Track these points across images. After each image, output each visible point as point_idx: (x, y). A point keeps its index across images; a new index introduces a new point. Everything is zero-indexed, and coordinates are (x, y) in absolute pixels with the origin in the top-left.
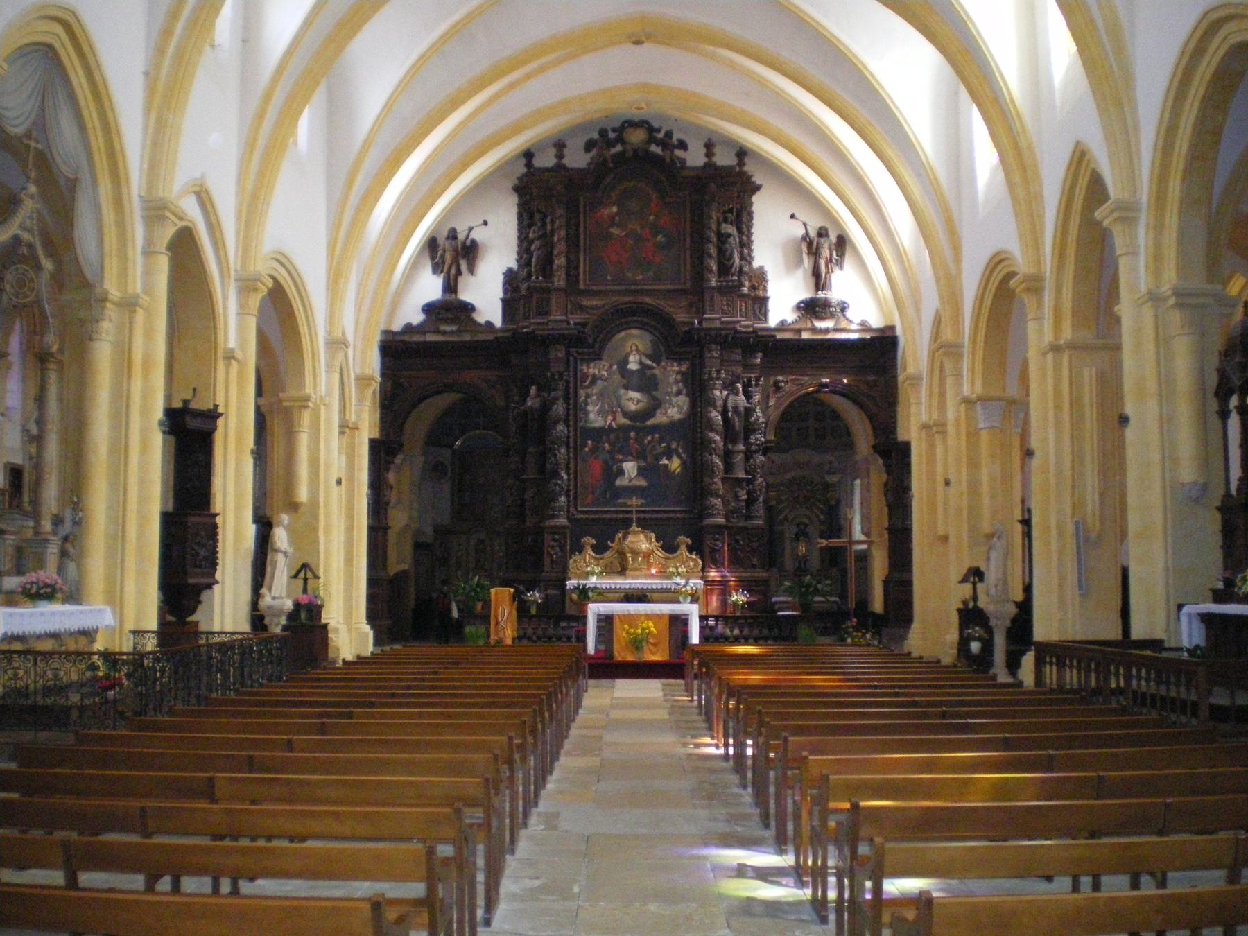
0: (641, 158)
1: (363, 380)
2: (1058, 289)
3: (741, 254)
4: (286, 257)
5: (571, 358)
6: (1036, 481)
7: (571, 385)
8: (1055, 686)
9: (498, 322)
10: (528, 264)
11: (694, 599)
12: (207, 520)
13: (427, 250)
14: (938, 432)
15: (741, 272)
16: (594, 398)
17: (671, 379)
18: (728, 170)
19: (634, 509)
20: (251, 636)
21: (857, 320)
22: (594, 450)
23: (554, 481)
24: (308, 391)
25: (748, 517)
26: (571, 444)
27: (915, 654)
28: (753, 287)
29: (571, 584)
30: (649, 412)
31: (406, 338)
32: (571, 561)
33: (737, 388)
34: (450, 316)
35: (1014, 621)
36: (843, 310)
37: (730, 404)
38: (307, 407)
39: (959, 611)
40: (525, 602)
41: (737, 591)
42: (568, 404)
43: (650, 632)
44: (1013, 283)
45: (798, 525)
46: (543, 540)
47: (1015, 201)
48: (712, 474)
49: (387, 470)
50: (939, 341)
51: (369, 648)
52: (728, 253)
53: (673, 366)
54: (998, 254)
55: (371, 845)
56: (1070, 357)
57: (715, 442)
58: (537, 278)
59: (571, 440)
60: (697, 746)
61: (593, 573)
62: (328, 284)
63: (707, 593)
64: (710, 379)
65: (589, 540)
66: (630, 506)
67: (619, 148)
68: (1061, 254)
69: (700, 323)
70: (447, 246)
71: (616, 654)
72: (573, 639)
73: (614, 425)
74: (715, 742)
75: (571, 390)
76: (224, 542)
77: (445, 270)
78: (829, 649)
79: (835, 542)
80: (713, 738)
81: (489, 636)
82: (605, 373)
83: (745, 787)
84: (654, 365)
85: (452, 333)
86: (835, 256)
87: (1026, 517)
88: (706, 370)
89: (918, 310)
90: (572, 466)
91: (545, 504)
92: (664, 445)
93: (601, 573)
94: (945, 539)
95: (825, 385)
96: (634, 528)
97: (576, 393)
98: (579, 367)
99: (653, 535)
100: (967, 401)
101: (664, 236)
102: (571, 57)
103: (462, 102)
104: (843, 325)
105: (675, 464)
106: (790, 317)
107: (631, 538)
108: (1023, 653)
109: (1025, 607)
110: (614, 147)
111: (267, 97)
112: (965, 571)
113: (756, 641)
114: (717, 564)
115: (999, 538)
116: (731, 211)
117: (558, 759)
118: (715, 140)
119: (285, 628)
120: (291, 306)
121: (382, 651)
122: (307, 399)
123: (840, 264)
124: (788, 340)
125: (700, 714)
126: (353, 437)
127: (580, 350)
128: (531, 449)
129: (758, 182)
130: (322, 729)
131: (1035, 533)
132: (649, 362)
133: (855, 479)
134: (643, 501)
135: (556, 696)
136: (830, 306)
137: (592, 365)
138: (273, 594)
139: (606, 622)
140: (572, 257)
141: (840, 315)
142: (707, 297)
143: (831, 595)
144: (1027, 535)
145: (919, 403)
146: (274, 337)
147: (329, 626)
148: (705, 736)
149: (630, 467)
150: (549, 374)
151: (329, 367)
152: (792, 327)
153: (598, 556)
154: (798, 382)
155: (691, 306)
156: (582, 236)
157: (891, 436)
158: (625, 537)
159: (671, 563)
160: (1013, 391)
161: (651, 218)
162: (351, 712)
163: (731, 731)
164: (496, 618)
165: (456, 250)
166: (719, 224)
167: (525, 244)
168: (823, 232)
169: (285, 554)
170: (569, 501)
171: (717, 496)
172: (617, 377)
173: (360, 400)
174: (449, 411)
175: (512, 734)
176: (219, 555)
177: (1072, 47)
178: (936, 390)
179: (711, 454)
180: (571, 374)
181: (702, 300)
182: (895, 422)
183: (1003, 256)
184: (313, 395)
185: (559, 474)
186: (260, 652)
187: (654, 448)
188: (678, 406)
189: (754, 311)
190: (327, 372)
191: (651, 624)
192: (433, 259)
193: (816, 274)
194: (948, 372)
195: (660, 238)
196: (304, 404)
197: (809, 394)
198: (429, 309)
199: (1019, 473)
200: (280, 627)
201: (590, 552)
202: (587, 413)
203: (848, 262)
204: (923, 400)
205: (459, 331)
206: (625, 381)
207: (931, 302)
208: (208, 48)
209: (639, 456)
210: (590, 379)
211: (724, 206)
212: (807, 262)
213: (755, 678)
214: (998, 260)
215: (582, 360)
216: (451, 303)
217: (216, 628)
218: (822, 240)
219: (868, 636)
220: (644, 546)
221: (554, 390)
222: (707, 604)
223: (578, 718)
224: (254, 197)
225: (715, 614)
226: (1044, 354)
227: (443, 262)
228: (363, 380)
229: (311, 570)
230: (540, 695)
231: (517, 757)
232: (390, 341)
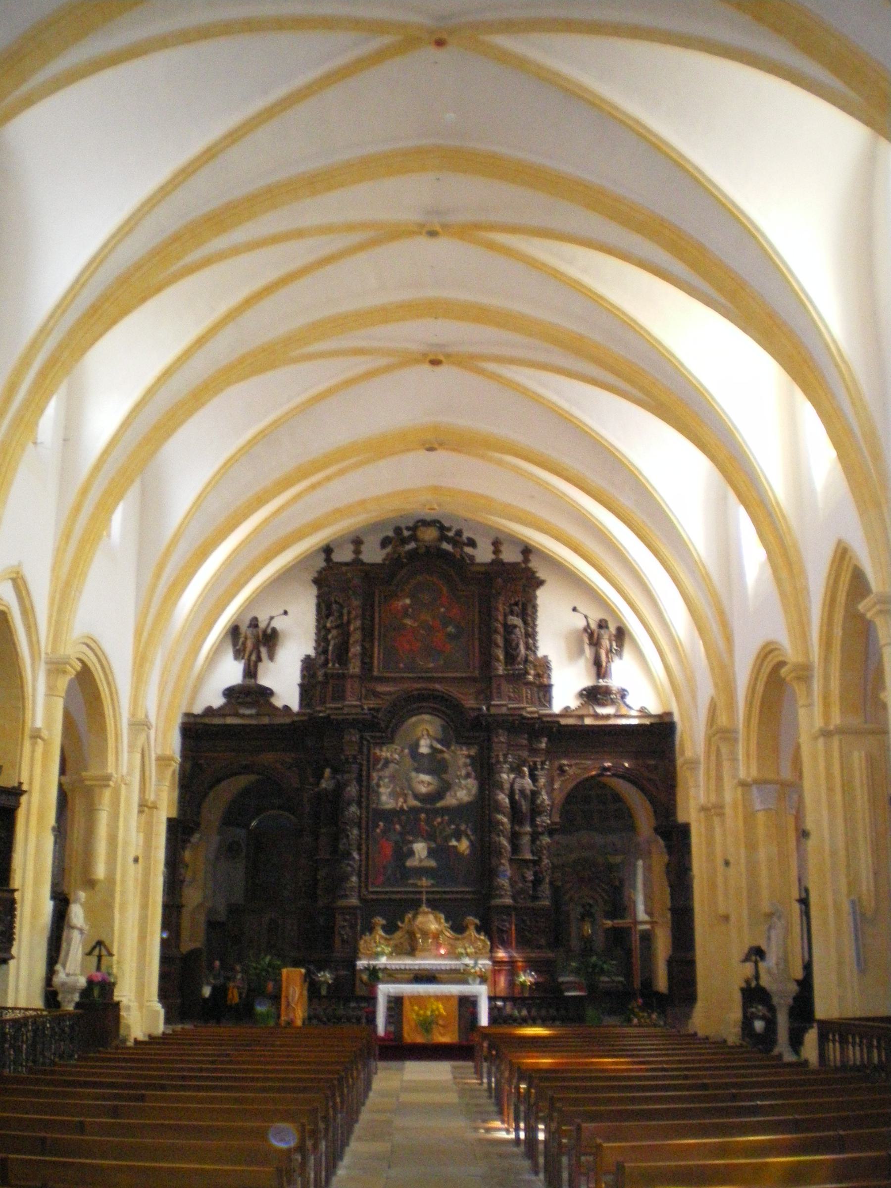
1: (163, 760)
2: (826, 678)
4: (95, 642)
5: (365, 743)
6: (812, 862)
7: (365, 768)
8: (838, 1064)
9: (295, 706)
10: (325, 652)
11: (483, 979)
12: (5, 895)
13: (230, 636)
15: (526, 661)
16: (386, 780)
18: (515, 565)
20: (45, 1013)
22: (384, 832)
23: (346, 862)
25: (535, 898)
27: (701, 1034)
28: (538, 675)
29: (361, 963)
30: (439, 795)
31: (207, 720)
32: (362, 942)
33: (523, 772)
35: (795, 999)
36: (623, 697)
37: (517, 787)
38: (108, 786)
39: (743, 990)
41: (525, 972)
42: (361, 786)
44: (783, 671)
45: (583, 906)
47: (783, 594)
49: (183, 848)
50: (715, 727)
51: (160, 1028)
52: (514, 644)
53: (461, 750)
54: (764, 648)
55: (448, 889)
56: (841, 741)
57: (502, 824)
58: (334, 665)
60: (488, 1130)
61: (382, 953)
63: (496, 973)
64: (498, 762)
65: (380, 921)
66: (422, 887)
68: (827, 643)
69: (488, 709)
70: (249, 635)
71: (405, 1035)
72: (364, 1020)
73: (405, 807)
74: (506, 1126)
75: (364, 773)
76: (21, 916)
78: (617, 1030)
79: (619, 922)
80: (503, 1122)
81: (279, 1016)
82: (396, 756)
83: (536, 1173)
84: (444, 749)
86: (614, 646)
87: (804, 895)
88: (493, 755)
89: (694, 697)
90: (364, 847)
91: (337, 884)
92: (453, 827)
93: (391, 953)
94: (726, 918)
96: (424, 908)
97: (369, 777)
98: (372, 751)
99: (442, 916)
100: (743, 784)
102: (368, 461)
103: (267, 501)
104: (624, 711)
105: (464, 846)
106: (574, 703)
107: (420, 919)
108: (804, 1030)
109: (806, 984)
110: (408, 544)
111: (85, 491)
112: (746, 950)
113: (544, 1022)
114: (505, 944)
115: (779, 918)
117: (348, 1144)
119: (78, 1005)
121: (174, 1031)
122: (108, 778)
123: (619, 653)
124: (571, 726)
125: (490, 1097)
126: (151, 816)
130: (115, 1112)
131: (814, 912)
132: (439, 746)
134: (432, 882)
135: (348, 1081)
137: (384, 749)
138: (67, 971)
139: (396, 1003)
142: (494, 685)
143: (616, 975)
144: (806, 913)
145: (697, 786)
146: (81, 719)
147: (121, 1005)
148: (496, 1120)
149: (420, 848)
150: (343, 757)
151: (131, 747)
153: (388, 937)
154: (582, 766)
157: (672, 818)
158: (415, 917)
159: (459, 943)
160: (787, 774)
162: (143, 1095)
163: (522, 1115)
164: (287, 997)
165: (257, 637)
166: (505, 616)
167: (323, 633)
168: (603, 624)
169: (81, 931)
170: (360, 881)
172: (408, 761)
173: (160, 780)
174: (246, 792)
175: (304, 1120)
176: (16, 931)
177: (832, 453)
178: (713, 774)
179: (499, 835)
180: (365, 758)
181: (489, 687)
183: (772, 647)
186: (52, 1028)
188: (467, 788)
189: (539, 698)
190: (129, 752)
191: (441, 1006)
192: (235, 644)
193: (597, 663)
194: (724, 757)
195: (451, 629)
196: (105, 783)
197: (593, 777)
198: (230, 693)
199: (795, 853)
200: (73, 1004)
201: (381, 932)
202: (378, 795)
203: (628, 653)
204: (702, 784)
205: (258, 715)
206: (416, 765)
207: (706, 690)
208: (31, 445)
209: (429, 837)
212: (588, 652)
213: (546, 1061)
214: (768, 651)
215: (376, 744)
217: (10, 1004)
218: (602, 631)
219: (654, 1016)
220: (434, 926)
221: (349, 772)
222: (495, 984)
223: (369, 1102)
224: (68, 584)
225: (502, 994)
226: (815, 738)
227: (244, 650)
228: (163, 760)
229: (105, 947)
230: (332, 1079)
231: (309, 1144)
232: (189, 724)
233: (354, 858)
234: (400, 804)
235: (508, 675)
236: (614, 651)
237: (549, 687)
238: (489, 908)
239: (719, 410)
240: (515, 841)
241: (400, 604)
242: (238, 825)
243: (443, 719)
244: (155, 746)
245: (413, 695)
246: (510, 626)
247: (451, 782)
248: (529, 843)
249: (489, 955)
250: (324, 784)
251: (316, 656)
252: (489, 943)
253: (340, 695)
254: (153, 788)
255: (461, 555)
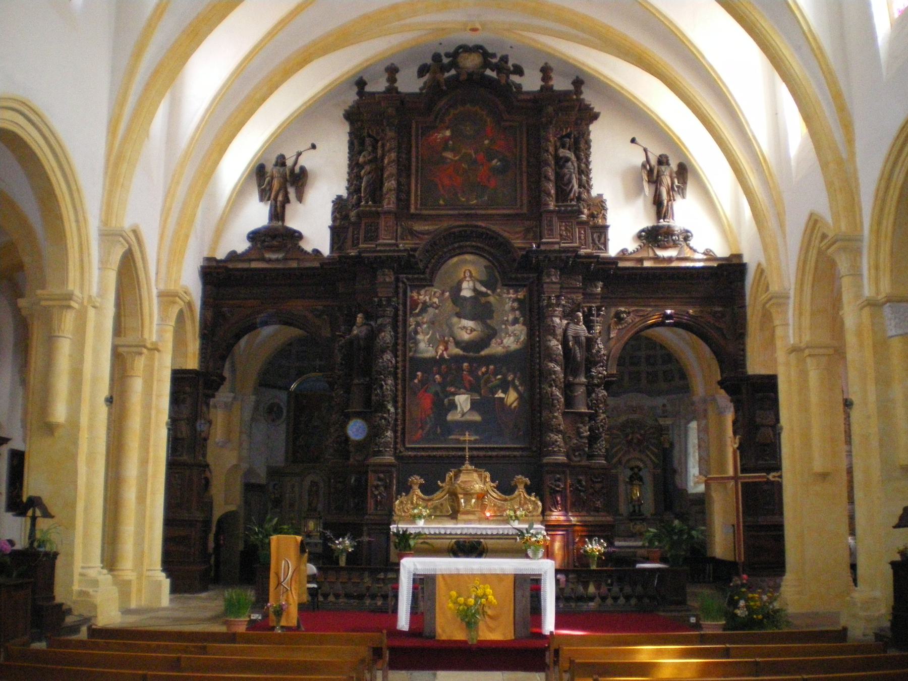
0: (476, 80)
3: (580, 180)
5: (401, 285)
7: (401, 313)
9: (326, 251)
14: (810, 355)
15: (579, 199)
16: (425, 326)
17: (508, 307)
19: (467, 446)
21: (701, 249)
22: (423, 382)
24: (71, 287)
25: (590, 457)
26: (400, 376)
28: (592, 216)
31: (230, 266)
32: (397, 502)
33: (578, 317)
34: (275, 243)
36: (686, 239)
37: (570, 333)
38: (69, 307)
40: (332, 551)
42: (396, 332)
43: (490, 603)
45: (632, 469)
46: (366, 480)
48: (552, 407)
53: (508, 293)
57: (555, 372)
58: (367, 202)
59: (399, 371)
61: (420, 516)
62: (107, 167)
64: (550, 305)
65: (417, 480)
67: (453, 72)
69: (538, 246)
70: (276, 174)
71: (439, 630)
73: (446, 356)
75: (400, 318)
77: (272, 197)
82: (436, 300)
84: (489, 292)
85: (277, 260)
86: (676, 183)
88: (544, 296)
89: (782, 225)
90: (400, 399)
92: (499, 377)
95: (670, 317)
96: (468, 466)
97: (405, 321)
98: (409, 293)
99: (488, 474)
100: (873, 305)
101: (500, 160)
104: (687, 253)
105: (511, 398)
106: (632, 246)
107: (463, 477)
110: (448, 72)
116: (568, 136)
118: (552, 64)
120: (48, 179)
123: (682, 191)
124: (633, 268)
126: (151, 359)
127: (410, 276)
128: (356, 381)
129: (596, 110)
132: (483, 289)
133: (689, 422)
134: (477, 437)
136: (673, 235)
137: (422, 292)
140: (403, 180)
141: (683, 244)
149: (463, 400)
150: (376, 299)
152: (633, 256)
153: (426, 497)
154: (641, 313)
155: (528, 230)
156: (414, 159)
158: (457, 476)
159: (508, 505)
161: (486, 142)
164: (277, 575)
165: (284, 177)
166: (556, 150)
168: (664, 160)
170: (396, 437)
171: (559, 432)
172: (449, 305)
173: (163, 319)
179: (551, 386)
180: (401, 301)
182: (744, 356)
184: (77, 292)
185: (386, 407)
187: (488, 381)
188: (515, 335)
189: (593, 240)
191: (489, 591)
192: (259, 185)
193: (658, 202)
196: (65, 303)
198: (255, 236)
201: (418, 492)
202: (416, 343)
204: (791, 322)
205: (285, 259)
206: (458, 310)
210: (420, 306)
211: (562, 129)
212: (648, 190)
215: (413, 287)
216: (276, 229)
218: (663, 168)
227: (271, 190)
232: (209, 267)
233: (389, 410)
234: (440, 352)
235: (559, 212)
236: (676, 189)
237: (605, 228)
238: (542, 466)
239: (713, 74)
240: (568, 392)
241: (440, 136)
242: (280, 388)
243: (488, 260)
244: (156, 281)
245: (454, 233)
246: (562, 158)
247: (497, 328)
248: (584, 395)
249: (541, 518)
250: (355, 331)
251: (348, 197)
252: (540, 503)
253: (372, 235)
254: (155, 328)
255: (506, 81)
